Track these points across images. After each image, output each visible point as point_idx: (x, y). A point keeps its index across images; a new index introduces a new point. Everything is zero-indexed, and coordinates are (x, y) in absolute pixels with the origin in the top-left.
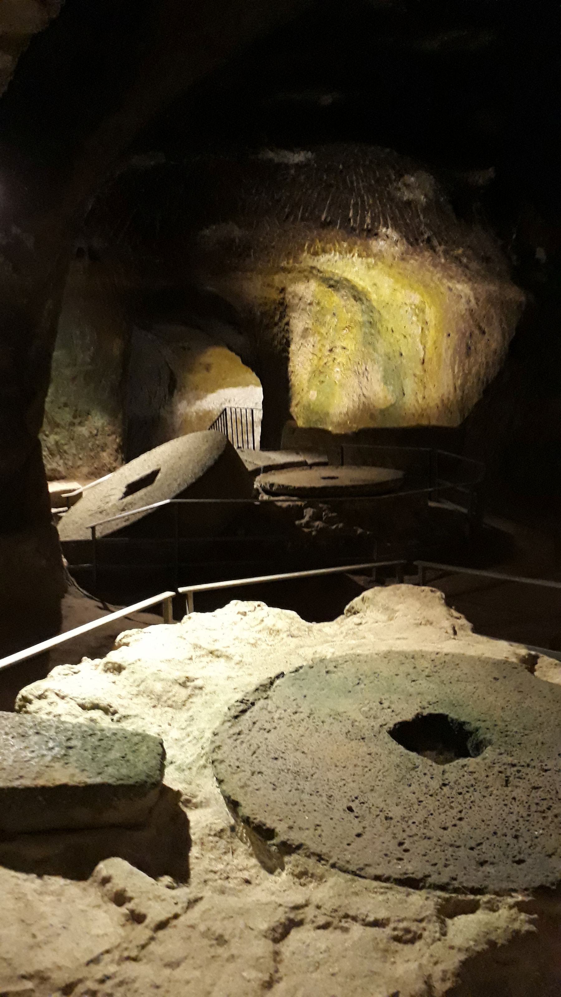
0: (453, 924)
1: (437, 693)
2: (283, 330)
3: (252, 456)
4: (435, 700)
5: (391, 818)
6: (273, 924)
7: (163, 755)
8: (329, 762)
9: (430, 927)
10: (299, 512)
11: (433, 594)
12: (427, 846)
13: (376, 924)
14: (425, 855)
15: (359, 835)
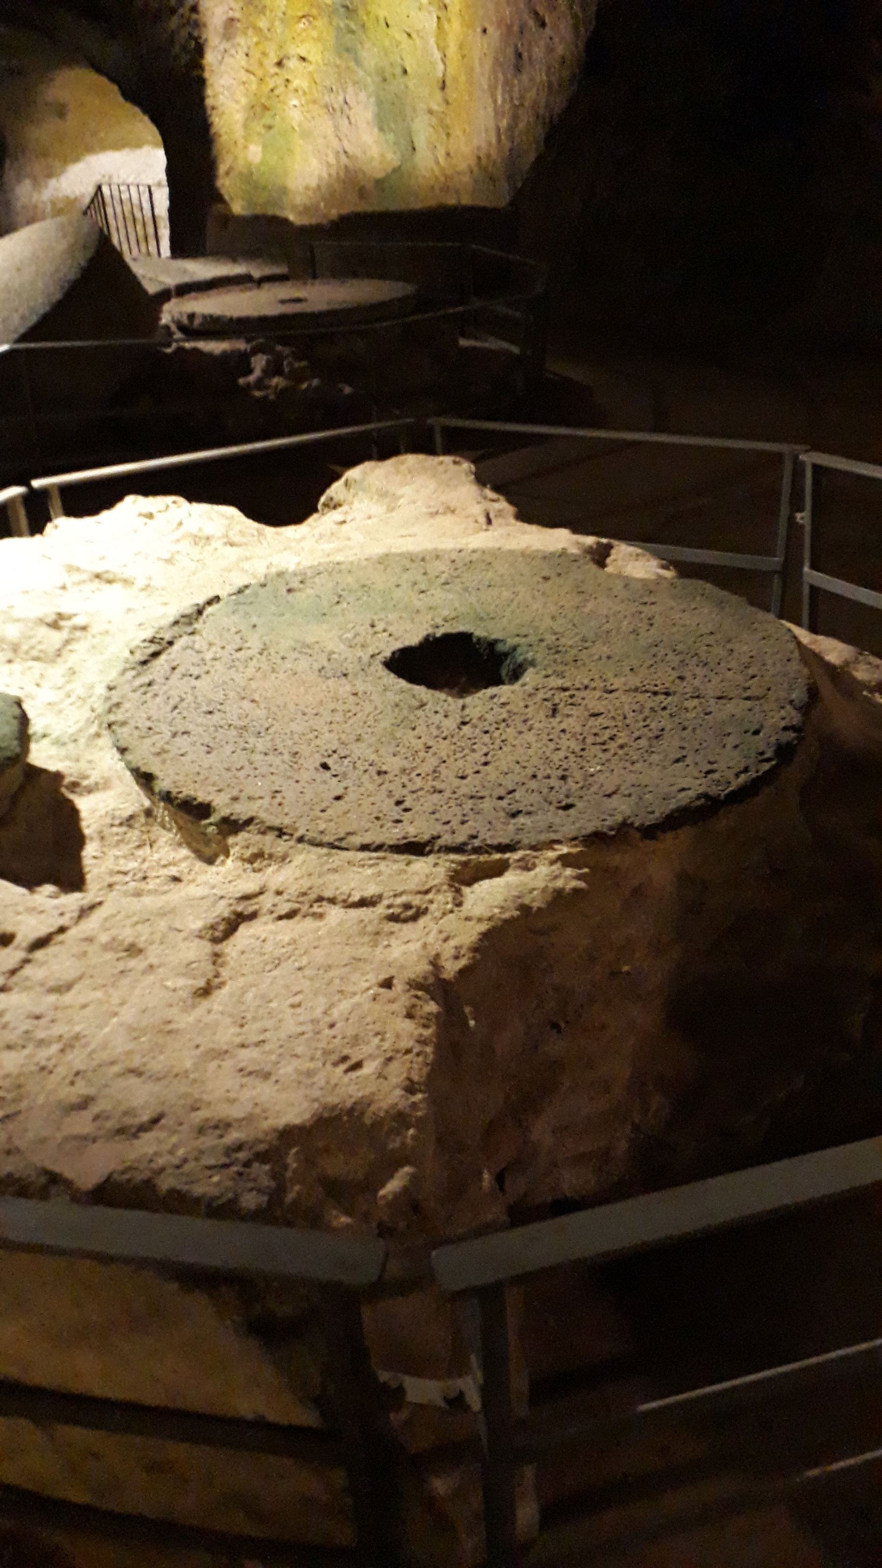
0: (472, 892)
1: (457, 605)
2: (188, 22)
3: (155, 265)
4: (453, 614)
5: (386, 773)
6: (210, 921)
7: (24, 720)
8: (292, 710)
9: (440, 898)
10: (242, 362)
11: (456, 467)
12: (435, 801)
13: (363, 903)
14: (434, 813)
15: (338, 798)
